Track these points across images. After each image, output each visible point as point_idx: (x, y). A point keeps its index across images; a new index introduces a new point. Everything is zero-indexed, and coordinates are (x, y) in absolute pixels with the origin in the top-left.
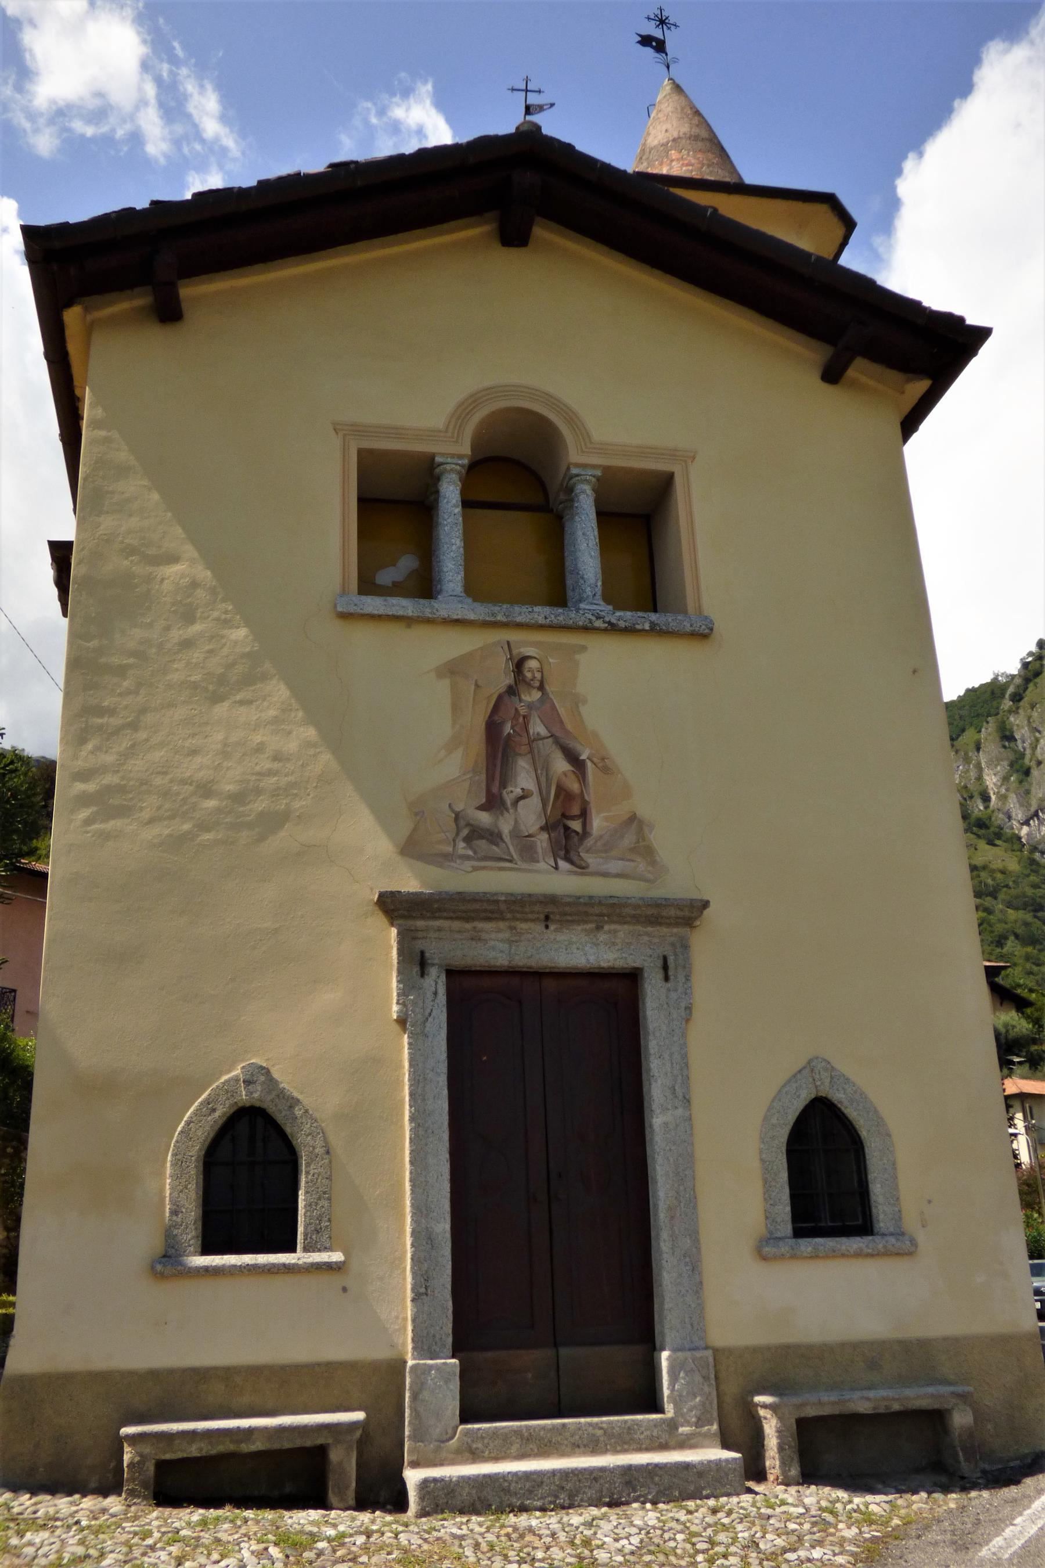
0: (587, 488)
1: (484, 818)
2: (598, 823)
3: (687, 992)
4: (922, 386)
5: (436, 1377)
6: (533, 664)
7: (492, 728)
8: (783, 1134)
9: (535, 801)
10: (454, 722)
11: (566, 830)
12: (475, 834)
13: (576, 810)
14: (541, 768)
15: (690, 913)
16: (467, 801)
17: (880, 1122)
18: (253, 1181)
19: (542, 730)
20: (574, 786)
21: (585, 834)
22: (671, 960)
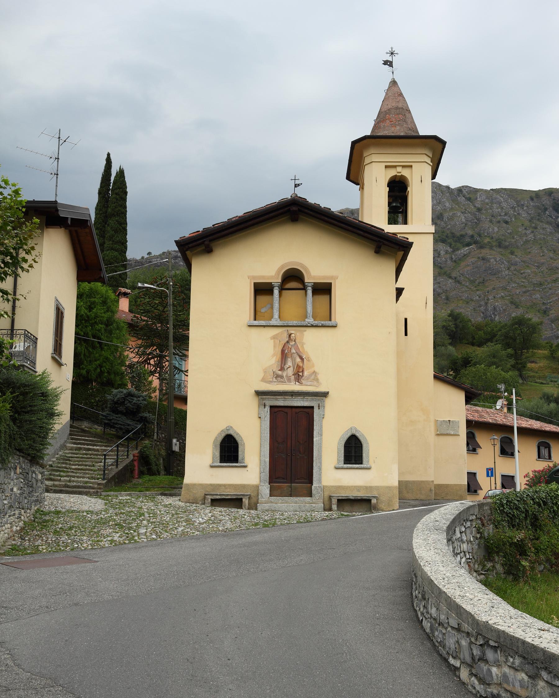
0: (310, 288)
1: (280, 373)
2: (306, 373)
3: (324, 411)
4: (401, 253)
5: (265, 490)
6: (293, 335)
7: (283, 351)
8: (343, 443)
9: (292, 368)
10: (274, 350)
11: (298, 376)
12: (277, 376)
13: (301, 370)
14: (294, 360)
15: (325, 395)
16: (276, 369)
17: (366, 440)
18: (229, 450)
19: (294, 352)
20: (301, 364)
21: (303, 376)
22: (320, 405)
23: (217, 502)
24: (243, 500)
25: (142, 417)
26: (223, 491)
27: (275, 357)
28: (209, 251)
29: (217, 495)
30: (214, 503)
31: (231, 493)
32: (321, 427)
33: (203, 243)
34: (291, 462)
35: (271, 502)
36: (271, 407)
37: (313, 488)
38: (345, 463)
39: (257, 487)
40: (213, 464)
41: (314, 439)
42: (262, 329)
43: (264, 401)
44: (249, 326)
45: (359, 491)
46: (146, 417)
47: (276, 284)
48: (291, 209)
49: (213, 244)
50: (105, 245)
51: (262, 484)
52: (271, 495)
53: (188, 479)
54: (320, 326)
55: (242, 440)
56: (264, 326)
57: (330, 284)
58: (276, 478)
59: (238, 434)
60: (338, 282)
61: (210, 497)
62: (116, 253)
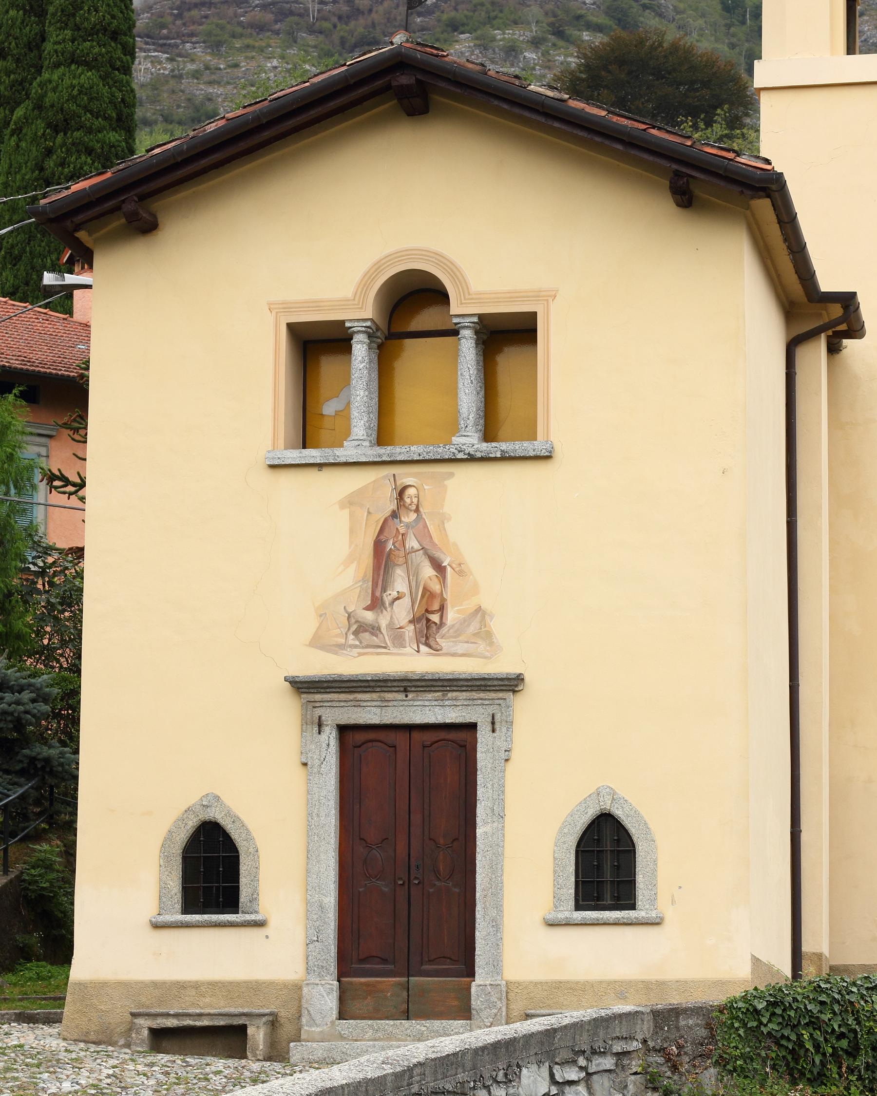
1: (369, 616)
2: (451, 616)
3: (509, 739)
5: (324, 997)
6: (411, 491)
7: (379, 545)
8: (572, 842)
9: (406, 601)
11: (427, 625)
12: (362, 628)
13: (436, 607)
14: (413, 574)
15: (512, 684)
16: (357, 604)
18: (212, 872)
19: (416, 545)
20: (436, 587)
21: (442, 624)
22: (498, 718)
23: (164, 1038)
24: (250, 1031)
25: (33, 760)
26: (193, 1005)
27: (354, 566)
28: (145, 227)
29: (167, 1015)
30: (165, 1044)
31: (212, 1009)
32: (501, 789)
33: (117, 208)
34: (407, 907)
35: (342, 1038)
36: (343, 730)
37: (473, 989)
38: (578, 907)
39: (296, 989)
40: (161, 919)
41: (479, 832)
42: (313, 473)
43: (318, 712)
44: (272, 467)
45: (622, 997)
46: (47, 760)
47: (357, 327)
48: (394, 83)
49: (157, 205)
50: (48, 47)
51: (314, 979)
52: (342, 1016)
53: (84, 966)
54: (495, 459)
55: (249, 838)
56: (320, 466)
57: (532, 317)
58: (362, 961)
59: (236, 819)
60: (554, 306)
61: (145, 1023)
62: (88, 77)
